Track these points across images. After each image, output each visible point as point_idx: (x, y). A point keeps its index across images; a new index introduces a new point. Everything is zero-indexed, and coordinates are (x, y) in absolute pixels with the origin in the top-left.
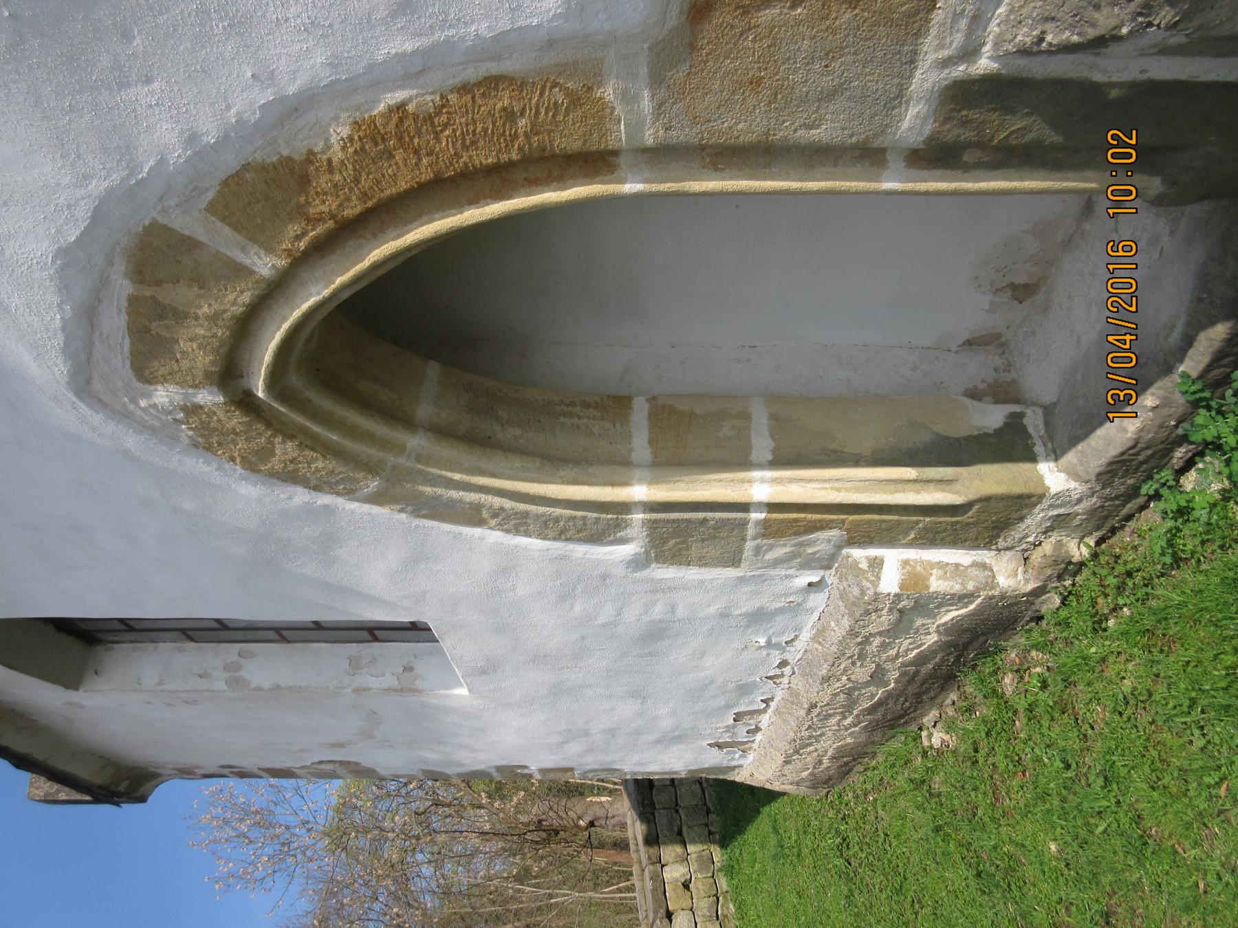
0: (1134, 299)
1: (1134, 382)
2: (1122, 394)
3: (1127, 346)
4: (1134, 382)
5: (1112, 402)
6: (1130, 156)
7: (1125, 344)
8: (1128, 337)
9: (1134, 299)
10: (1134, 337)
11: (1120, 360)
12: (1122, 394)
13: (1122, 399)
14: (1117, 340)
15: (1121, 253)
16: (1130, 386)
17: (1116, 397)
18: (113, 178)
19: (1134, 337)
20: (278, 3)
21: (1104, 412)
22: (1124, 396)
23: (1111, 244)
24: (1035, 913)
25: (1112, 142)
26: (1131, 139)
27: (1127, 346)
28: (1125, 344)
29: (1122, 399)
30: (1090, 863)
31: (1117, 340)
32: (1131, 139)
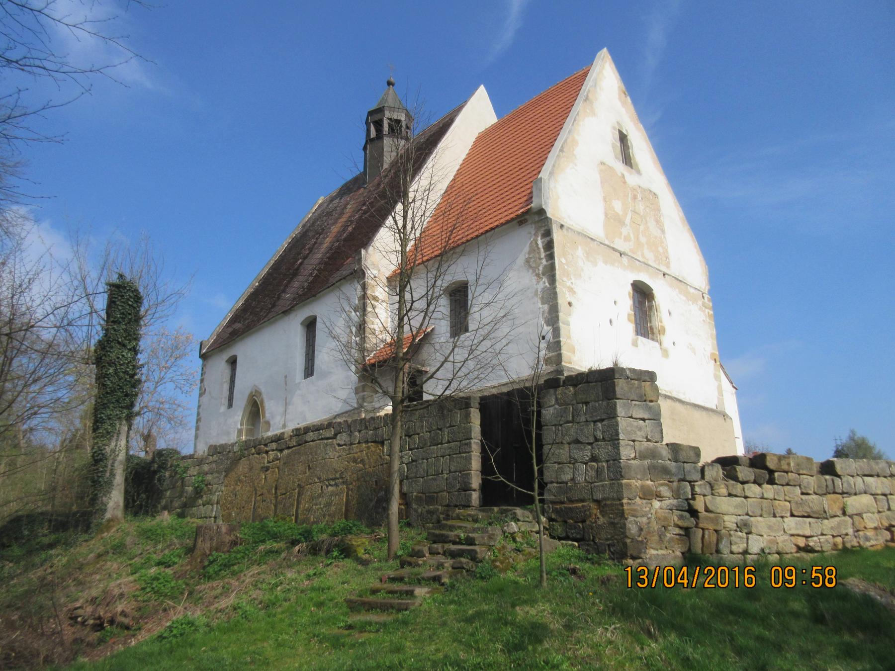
0: (713, 586)
1: (653, 586)
2: (644, 577)
3: (679, 581)
4: (653, 586)
5: (639, 570)
6: (777, 583)
7: (681, 579)
8: (685, 581)
9: (713, 586)
10: (686, 586)
11: (777, 579)
12: (644, 577)
13: (641, 577)
14: (683, 573)
15: (747, 576)
16: (650, 582)
17: (642, 573)
18: (94, 593)
19: (686, 586)
20: (503, 668)
21: (805, 567)
22: (644, 579)
23: (753, 569)
24: (370, 650)
25: (706, 570)
26: (708, 584)
27: (679, 581)
28: (681, 579)
29: (641, 577)
30: (642, 456)
31: (683, 573)
32: (708, 584)
